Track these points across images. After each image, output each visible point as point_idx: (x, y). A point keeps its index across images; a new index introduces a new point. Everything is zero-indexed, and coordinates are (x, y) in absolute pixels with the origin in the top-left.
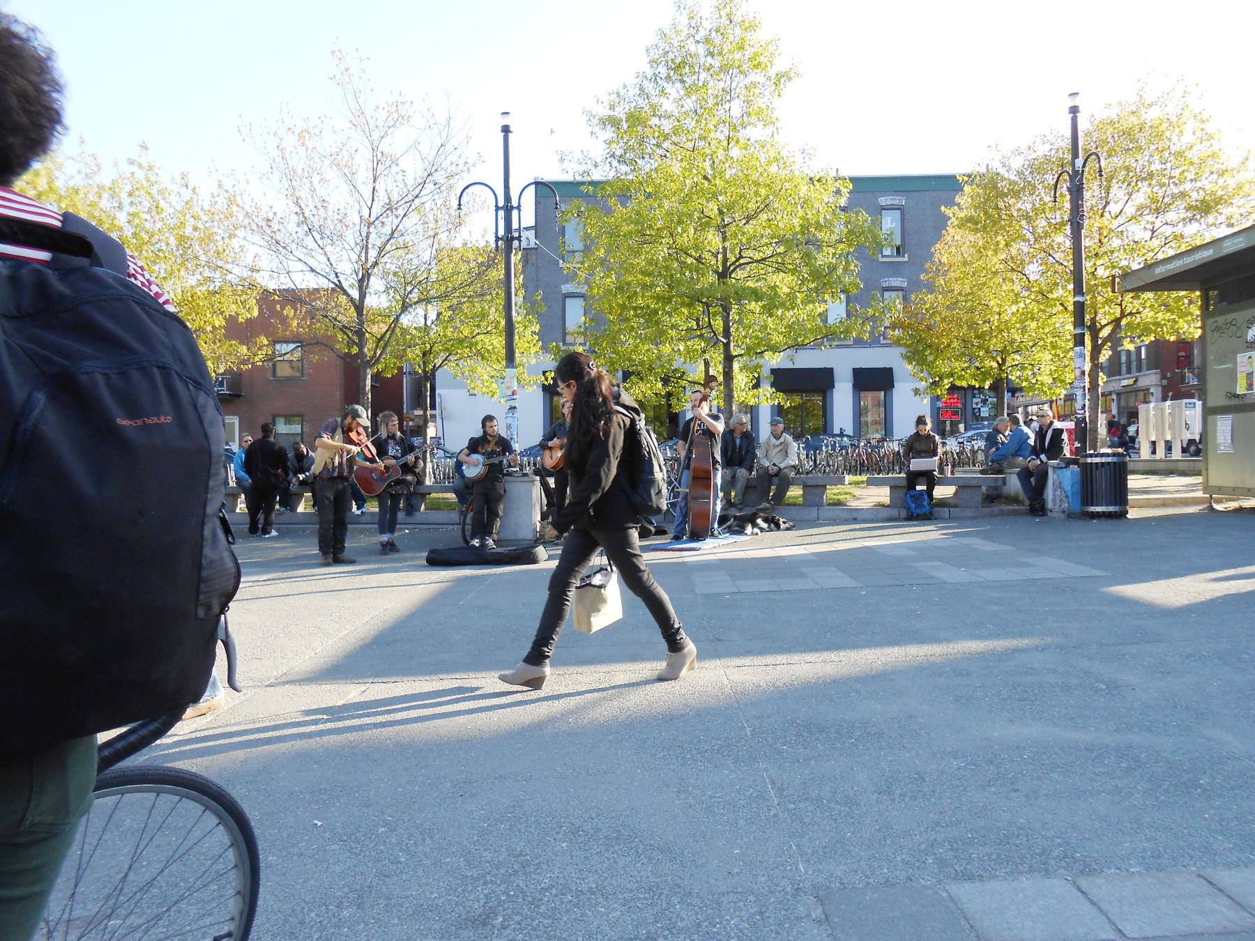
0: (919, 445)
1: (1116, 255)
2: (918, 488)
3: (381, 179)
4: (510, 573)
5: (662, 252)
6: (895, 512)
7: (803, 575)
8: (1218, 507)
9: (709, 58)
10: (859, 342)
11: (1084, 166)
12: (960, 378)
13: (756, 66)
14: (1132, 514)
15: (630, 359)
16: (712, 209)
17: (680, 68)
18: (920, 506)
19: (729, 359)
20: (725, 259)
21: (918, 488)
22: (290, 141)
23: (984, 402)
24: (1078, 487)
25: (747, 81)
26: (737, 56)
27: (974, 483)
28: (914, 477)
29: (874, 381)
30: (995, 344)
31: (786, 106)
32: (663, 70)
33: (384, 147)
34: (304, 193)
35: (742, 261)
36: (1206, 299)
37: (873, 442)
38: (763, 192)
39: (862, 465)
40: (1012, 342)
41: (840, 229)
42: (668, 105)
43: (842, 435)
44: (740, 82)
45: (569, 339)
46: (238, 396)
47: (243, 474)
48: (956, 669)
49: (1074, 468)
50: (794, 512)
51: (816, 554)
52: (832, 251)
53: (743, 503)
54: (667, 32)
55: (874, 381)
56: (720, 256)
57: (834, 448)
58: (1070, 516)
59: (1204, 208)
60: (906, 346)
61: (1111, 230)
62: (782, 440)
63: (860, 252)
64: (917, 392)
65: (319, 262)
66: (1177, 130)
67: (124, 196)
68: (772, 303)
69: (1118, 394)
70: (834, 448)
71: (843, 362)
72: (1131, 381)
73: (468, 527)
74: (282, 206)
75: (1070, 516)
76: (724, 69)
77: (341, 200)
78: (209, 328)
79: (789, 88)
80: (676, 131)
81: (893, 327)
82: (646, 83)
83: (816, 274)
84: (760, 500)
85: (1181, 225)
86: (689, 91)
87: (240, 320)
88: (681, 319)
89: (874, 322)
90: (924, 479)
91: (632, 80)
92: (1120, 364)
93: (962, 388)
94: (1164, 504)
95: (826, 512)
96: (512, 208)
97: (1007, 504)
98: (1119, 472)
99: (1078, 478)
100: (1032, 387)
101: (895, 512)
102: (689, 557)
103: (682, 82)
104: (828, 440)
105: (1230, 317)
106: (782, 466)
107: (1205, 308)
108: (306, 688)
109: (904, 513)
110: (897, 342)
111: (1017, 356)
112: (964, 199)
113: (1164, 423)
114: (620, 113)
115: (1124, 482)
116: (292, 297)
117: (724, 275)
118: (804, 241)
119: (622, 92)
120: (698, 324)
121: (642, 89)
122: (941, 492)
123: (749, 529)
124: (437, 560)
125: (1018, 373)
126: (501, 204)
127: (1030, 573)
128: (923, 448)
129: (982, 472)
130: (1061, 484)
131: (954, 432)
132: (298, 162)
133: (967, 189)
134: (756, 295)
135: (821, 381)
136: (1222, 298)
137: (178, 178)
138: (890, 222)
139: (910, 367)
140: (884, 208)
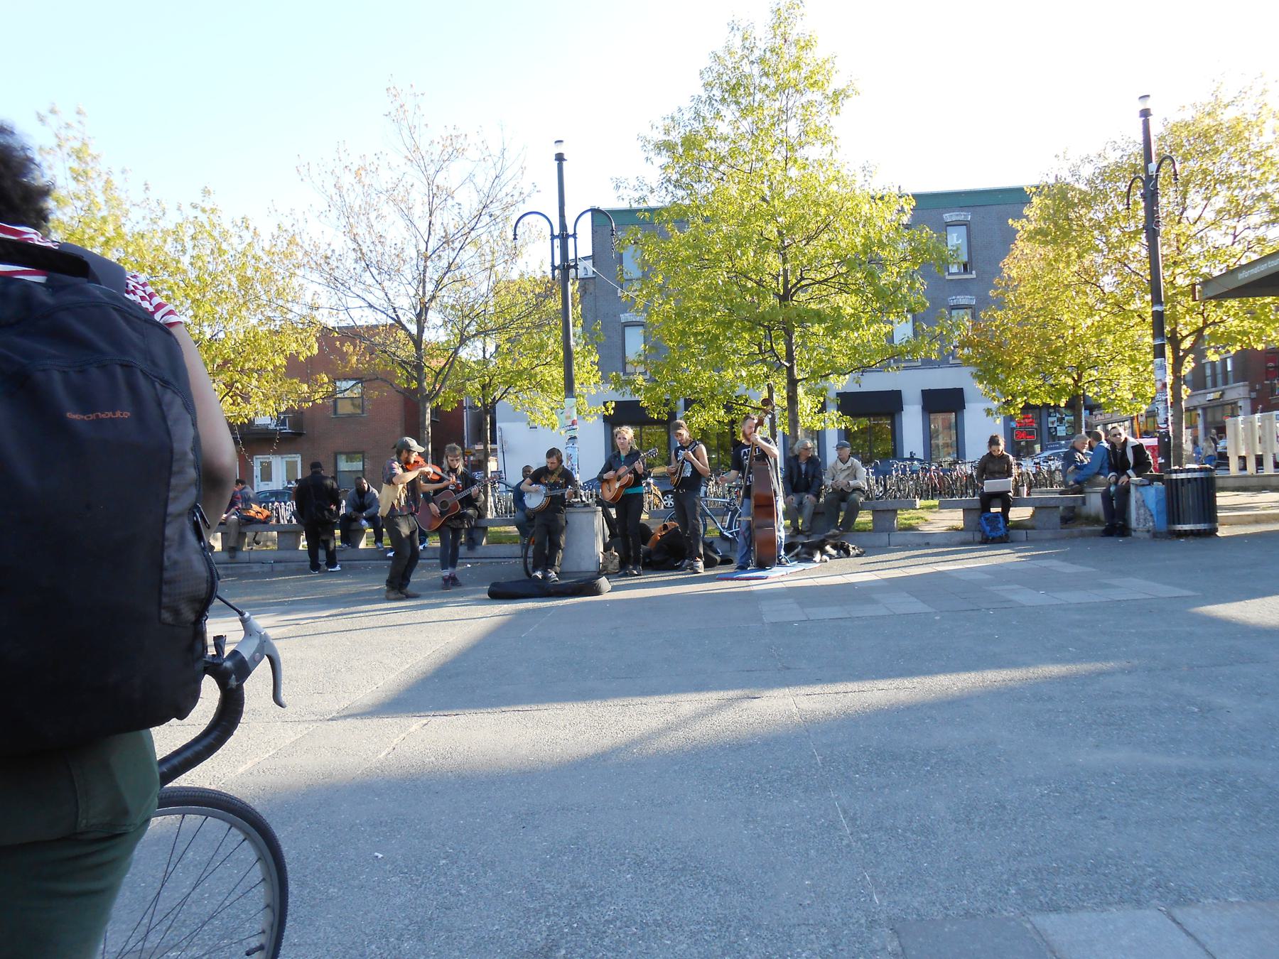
0: (993, 465)
2: (993, 510)
5: (721, 277)
10: (928, 363)
13: (812, 85)
14: (1222, 532)
15: (691, 387)
16: (771, 231)
17: (735, 89)
18: (994, 528)
19: (793, 383)
20: (786, 282)
21: (993, 510)
22: (347, 179)
23: (1061, 420)
24: (1163, 505)
25: (804, 100)
26: (793, 75)
27: (1052, 503)
28: (988, 499)
29: (944, 403)
30: (1069, 359)
32: (717, 93)
34: (361, 230)
35: (803, 283)
38: (823, 211)
39: (934, 489)
42: (723, 128)
43: (912, 459)
44: (797, 101)
46: (300, 434)
49: (1158, 484)
50: (864, 538)
55: (944, 403)
56: (781, 279)
57: (904, 472)
58: (1156, 535)
60: (976, 364)
65: (376, 297)
66: (1256, 130)
68: (836, 324)
69: (1204, 409)
70: (904, 472)
71: (911, 384)
72: (1217, 395)
74: (341, 244)
75: (1156, 535)
76: (781, 88)
78: (270, 367)
79: (848, 106)
80: (732, 153)
81: (962, 345)
83: (880, 294)
90: (998, 501)
91: (686, 103)
92: (1205, 377)
93: (1036, 407)
94: (1257, 520)
95: (897, 538)
96: (568, 236)
98: (1206, 489)
99: (1163, 496)
100: (1111, 403)
101: (968, 536)
102: (756, 586)
103: (737, 103)
108: (368, 721)
109: (978, 537)
110: (967, 361)
111: (1093, 372)
114: (675, 137)
116: (351, 334)
117: (785, 297)
118: (867, 261)
119: (677, 116)
121: (697, 113)
122: (1016, 514)
123: (818, 557)
124: (499, 594)
125: (1096, 389)
126: (557, 232)
127: (1116, 595)
128: (996, 468)
129: (1061, 493)
131: (1029, 452)
132: (355, 199)
134: (819, 317)
135: (889, 404)
138: (956, 239)
139: (981, 386)
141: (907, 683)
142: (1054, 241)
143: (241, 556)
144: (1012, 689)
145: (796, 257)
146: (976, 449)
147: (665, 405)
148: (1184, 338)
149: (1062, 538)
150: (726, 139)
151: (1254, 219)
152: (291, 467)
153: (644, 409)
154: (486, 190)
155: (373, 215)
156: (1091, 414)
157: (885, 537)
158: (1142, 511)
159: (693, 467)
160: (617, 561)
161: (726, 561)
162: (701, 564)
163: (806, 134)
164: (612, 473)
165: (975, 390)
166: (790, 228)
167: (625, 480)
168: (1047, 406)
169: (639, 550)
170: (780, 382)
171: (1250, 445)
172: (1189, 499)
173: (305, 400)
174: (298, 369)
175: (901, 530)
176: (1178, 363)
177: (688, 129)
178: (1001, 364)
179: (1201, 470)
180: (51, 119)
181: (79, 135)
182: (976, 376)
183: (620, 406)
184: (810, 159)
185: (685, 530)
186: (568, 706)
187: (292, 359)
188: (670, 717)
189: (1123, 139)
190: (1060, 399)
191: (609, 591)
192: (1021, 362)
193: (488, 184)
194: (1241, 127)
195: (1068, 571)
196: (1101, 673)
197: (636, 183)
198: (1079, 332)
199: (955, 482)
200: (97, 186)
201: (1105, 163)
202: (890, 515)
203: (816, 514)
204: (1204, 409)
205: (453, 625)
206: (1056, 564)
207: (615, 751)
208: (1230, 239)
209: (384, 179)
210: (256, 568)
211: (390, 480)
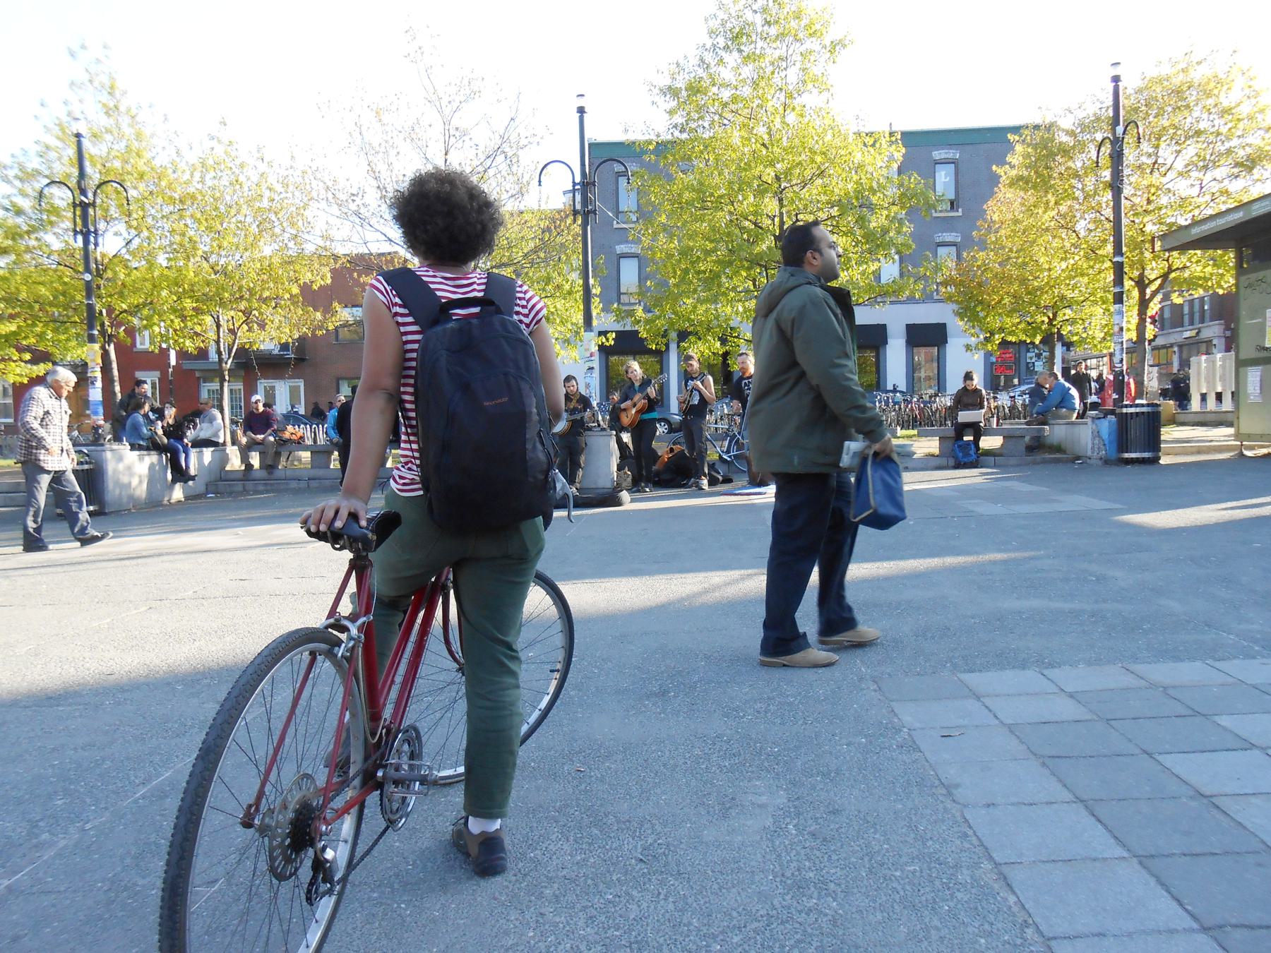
0: (968, 398)
1: (1163, 211)
2: (966, 438)
3: (451, 152)
5: (722, 217)
8: (1249, 453)
9: (766, 27)
10: (911, 300)
14: (1164, 460)
15: (689, 320)
17: (737, 37)
18: (967, 455)
20: (782, 223)
21: (966, 438)
23: (1039, 356)
24: (1114, 437)
25: (803, 49)
26: (793, 24)
27: (1018, 434)
28: (961, 429)
29: (927, 337)
30: (1046, 299)
33: (455, 122)
34: (381, 167)
36: (1240, 259)
37: (926, 398)
38: (819, 159)
39: (915, 419)
40: (1063, 298)
41: (892, 192)
42: (726, 74)
43: (895, 390)
45: (624, 299)
46: (303, 360)
47: (332, 432)
48: (982, 569)
49: (1112, 418)
52: (885, 212)
55: (927, 337)
56: (777, 220)
57: (887, 404)
58: (1107, 462)
59: (1248, 165)
60: (957, 302)
61: (1158, 188)
63: (912, 212)
64: (968, 347)
66: (1225, 87)
69: (1180, 346)
70: (887, 404)
72: (1193, 333)
75: (1107, 462)
76: (780, 37)
78: (287, 296)
79: (843, 56)
80: (735, 99)
81: (945, 284)
83: (869, 236)
85: (1226, 182)
87: (315, 287)
89: (926, 281)
90: (971, 430)
92: (1182, 315)
93: (1010, 343)
94: (1199, 451)
97: (1050, 453)
98: (1153, 422)
99: (1115, 427)
100: (1083, 341)
101: (943, 461)
103: (740, 51)
105: (1261, 274)
107: (1239, 266)
110: (950, 298)
111: (1068, 311)
113: (1210, 374)
114: (680, 83)
115: (1158, 434)
118: (860, 204)
119: (682, 62)
120: (754, 285)
121: (702, 60)
122: (987, 443)
127: (1058, 507)
128: (970, 401)
129: (1027, 424)
130: (1088, 435)
131: (1008, 386)
133: (1019, 148)
136: (1255, 257)
138: (944, 179)
141: (885, 564)
142: (1034, 187)
144: (965, 568)
145: (793, 201)
146: (954, 384)
148: (1151, 282)
151: (1220, 172)
152: (294, 392)
153: (643, 340)
155: (393, 152)
156: (1068, 350)
158: (1096, 441)
159: (701, 395)
160: (630, 479)
161: (727, 480)
162: (705, 482)
163: (804, 82)
164: (629, 403)
165: (956, 325)
166: (788, 172)
167: (639, 405)
169: (647, 471)
171: (1211, 381)
172: (1135, 430)
173: (321, 328)
174: (312, 297)
176: (1144, 304)
177: (692, 75)
178: (981, 302)
179: (1148, 405)
182: (957, 314)
183: (621, 335)
184: (808, 107)
185: (691, 454)
186: (624, 580)
187: (306, 289)
188: (706, 586)
189: (1097, 101)
190: (1035, 336)
194: (1212, 85)
196: (1031, 558)
197: (644, 128)
198: (1054, 274)
199: (934, 413)
200: (125, 121)
204: (1180, 346)
206: (1016, 485)
208: (1196, 190)
210: (293, 484)
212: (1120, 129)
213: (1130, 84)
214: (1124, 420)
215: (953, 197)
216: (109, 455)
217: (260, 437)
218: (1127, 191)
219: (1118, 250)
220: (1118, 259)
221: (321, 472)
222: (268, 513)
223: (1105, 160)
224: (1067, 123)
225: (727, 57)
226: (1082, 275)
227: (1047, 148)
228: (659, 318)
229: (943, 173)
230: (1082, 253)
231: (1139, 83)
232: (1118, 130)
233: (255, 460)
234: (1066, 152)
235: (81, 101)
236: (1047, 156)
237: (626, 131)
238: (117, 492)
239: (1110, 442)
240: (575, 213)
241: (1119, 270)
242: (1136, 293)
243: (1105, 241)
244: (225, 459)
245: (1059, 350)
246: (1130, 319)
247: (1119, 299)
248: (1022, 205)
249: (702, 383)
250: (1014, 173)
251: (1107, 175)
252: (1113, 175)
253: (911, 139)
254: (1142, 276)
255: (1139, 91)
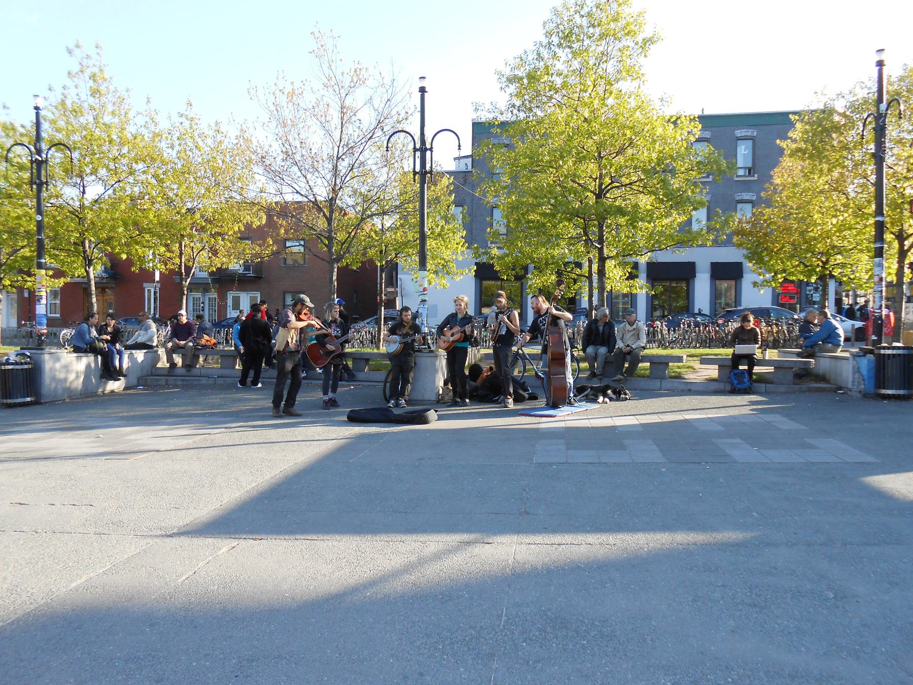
2: (741, 367)
4: (410, 430)
6: (721, 386)
7: (623, 447)
11: (887, 110)
12: (792, 274)
13: (627, 34)
16: (590, 144)
18: (741, 382)
19: (602, 260)
20: (601, 184)
21: (741, 367)
22: (283, 100)
23: (816, 289)
25: (620, 45)
26: (612, 25)
27: (787, 365)
29: (727, 273)
30: (820, 247)
31: (649, 64)
32: (555, 40)
35: (614, 185)
38: (628, 132)
42: (560, 66)
43: (700, 314)
44: (614, 48)
50: (643, 383)
51: (642, 425)
53: (603, 375)
54: (559, 9)
55: (727, 273)
57: (689, 326)
60: (747, 249)
62: (635, 326)
65: (302, 186)
67: (175, 138)
68: (634, 216)
70: (689, 326)
71: (703, 257)
73: (388, 391)
74: (276, 149)
75: (866, 395)
76: (602, 36)
77: (318, 141)
79: (653, 49)
82: (541, 49)
84: (615, 374)
86: (575, 54)
88: (571, 230)
90: (746, 361)
91: (531, 47)
93: (792, 281)
95: (667, 384)
96: (426, 149)
99: (873, 365)
101: (721, 386)
102: (545, 424)
104: (686, 320)
106: (634, 346)
108: (195, 540)
109: (728, 387)
111: (839, 257)
112: (797, 132)
114: (521, 73)
116: (284, 210)
117: (600, 194)
118: (661, 170)
119: (524, 57)
121: (539, 54)
123: (601, 399)
124: (355, 418)
125: (840, 270)
126: (418, 146)
127: (813, 456)
129: (799, 355)
132: (288, 113)
133: (799, 126)
134: (621, 211)
135: (687, 271)
137: (213, 125)
138: (744, 153)
139: (751, 265)
140: (739, 139)
143: (194, 371)
147: (513, 270)
149: (794, 392)
150: (561, 75)
154: (380, 110)
157: (657, 383)
158: (857, 376)
162: (511, 401)
168: (801, 281)
170: (594, 254)
174: (249, 234)
175: (672, 377)
178: (766, 249)
179: (903, 348)
180: (77, 51)
181: (97, 64)
190: (810, 276)
191: (435, 423)
192: (781, 249)
193: (382, 105)
195: (785, 427)
197: (490, 107)
199: (727, 335)
201: (855, 99)
202: (662, 367)
203: (606, 363)
205: (311, 441)
207: (355, 590)
209: (308, 100)
210: (204, 381)
211: (285, 324)
212: (883, 106)
213: (892, 71)
214: (881, 361)
215: (750, 165)
216: (47, 357)
217: (183, 343)
218: (889, 160)
219: (879, 211)
220: (879, 219)
221: (227, 372)
222: (147, 411)
223: (869, 135)
224: (840, 106)
225: (560, 52)
226: (850, 229)
227: (823, 124)
228: (507, 255)
229: (743, 147)
230: (851, 210)
231: (900, 72)
232: (880, 112)
233: (178, 360)
234: (837, 128)
235: (76, 87)
236: (822, 132)
237: (476, 110)
238: (53, 385)
239: (869, 378)
240: (415, 173)
241: (880, 228)
242: (896, 244)
243: (869, 202)
244: (157, 359)
245: (832, 286)
246: (891, 265)
247: (879, 253)
248: (802, 171)
249: (508, 318)
250: (794, 146)
251: (872, 147)
252: (876, 146)
253: (706, 121)
254: (901, 231)
255: (902, 79)
